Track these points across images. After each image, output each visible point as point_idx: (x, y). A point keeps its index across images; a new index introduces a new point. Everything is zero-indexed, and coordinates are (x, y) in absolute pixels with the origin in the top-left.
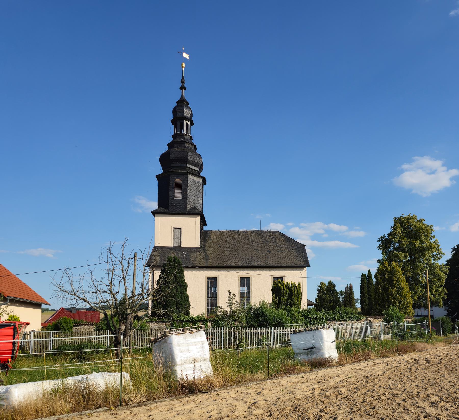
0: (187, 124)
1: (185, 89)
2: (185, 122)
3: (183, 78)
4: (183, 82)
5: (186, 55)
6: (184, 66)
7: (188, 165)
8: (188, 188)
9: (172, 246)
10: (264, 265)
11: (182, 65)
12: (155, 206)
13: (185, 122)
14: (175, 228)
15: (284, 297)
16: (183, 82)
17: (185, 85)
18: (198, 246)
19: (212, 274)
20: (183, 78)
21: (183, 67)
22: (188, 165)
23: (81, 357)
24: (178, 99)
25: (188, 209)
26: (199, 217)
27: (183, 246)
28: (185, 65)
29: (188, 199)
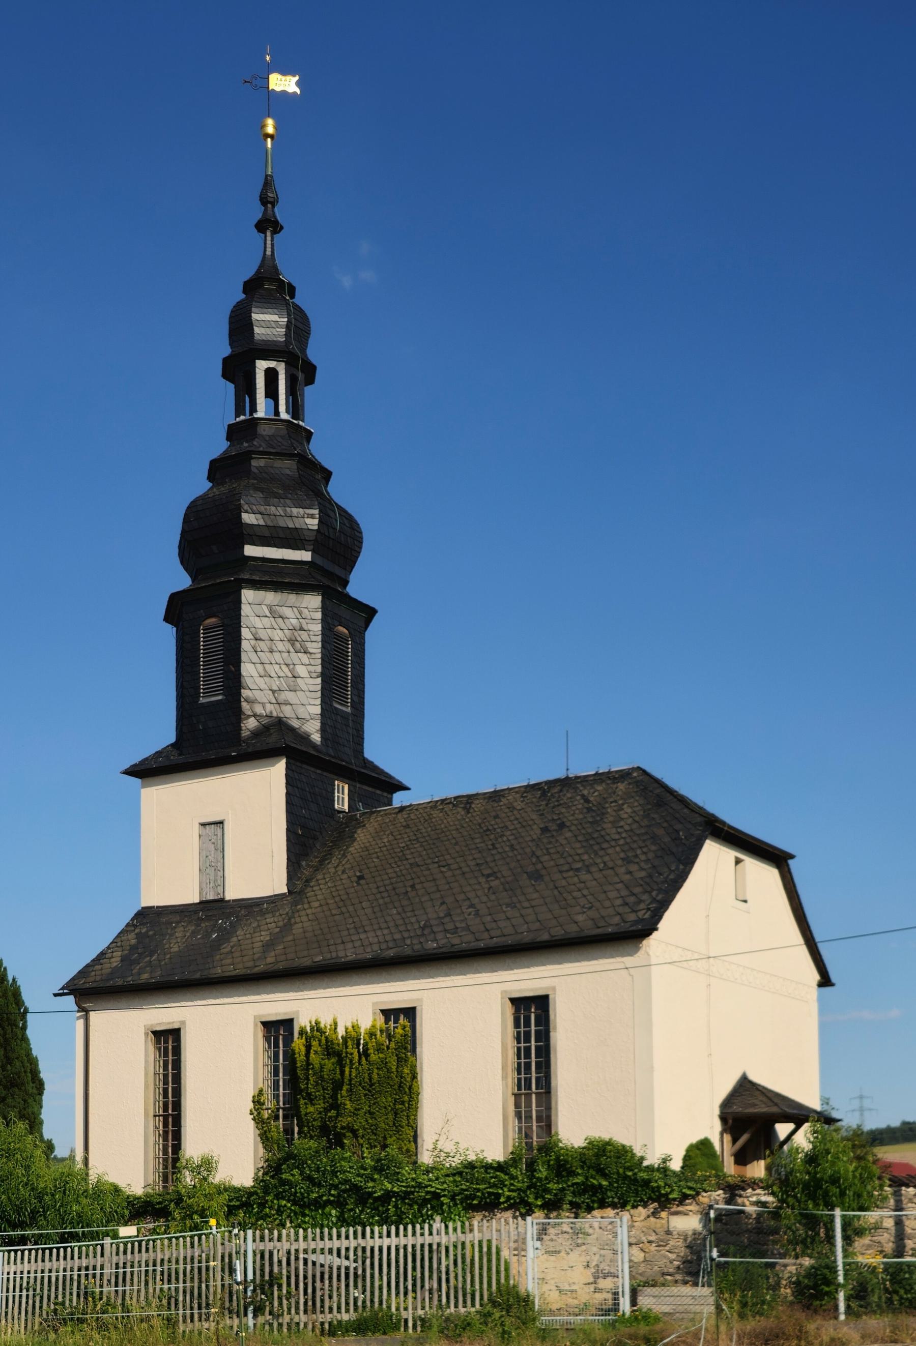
0: (271, 375)
1: (277, 228)
2: (261, 365)
3: (268, 183)
4: (267, 200)
5: (283, 83)
6: (270, 129)
7: (251, 551)
8: (245, 645)
9: (197, 901)
10: (590, 930)
11: (264, 126)
12: (162, 732)
13: (261, 365)
14: (203, 825)
15: (310, 1099)
16: (267, 200)
17: (279, 213)
18: (284, 890)
19: (528, 979)
20: (268, 183)
21: (267, 136)
22: (251, 551)
23: (360, 1329)
24: (249, 272)
25: (245, 734)
26: (281, 766)
27: (230, 895)
28: (276, 128)
29: (245, 693)
